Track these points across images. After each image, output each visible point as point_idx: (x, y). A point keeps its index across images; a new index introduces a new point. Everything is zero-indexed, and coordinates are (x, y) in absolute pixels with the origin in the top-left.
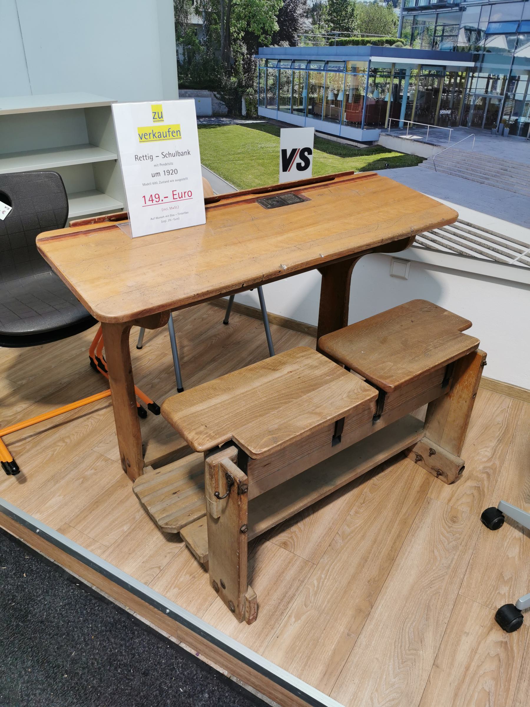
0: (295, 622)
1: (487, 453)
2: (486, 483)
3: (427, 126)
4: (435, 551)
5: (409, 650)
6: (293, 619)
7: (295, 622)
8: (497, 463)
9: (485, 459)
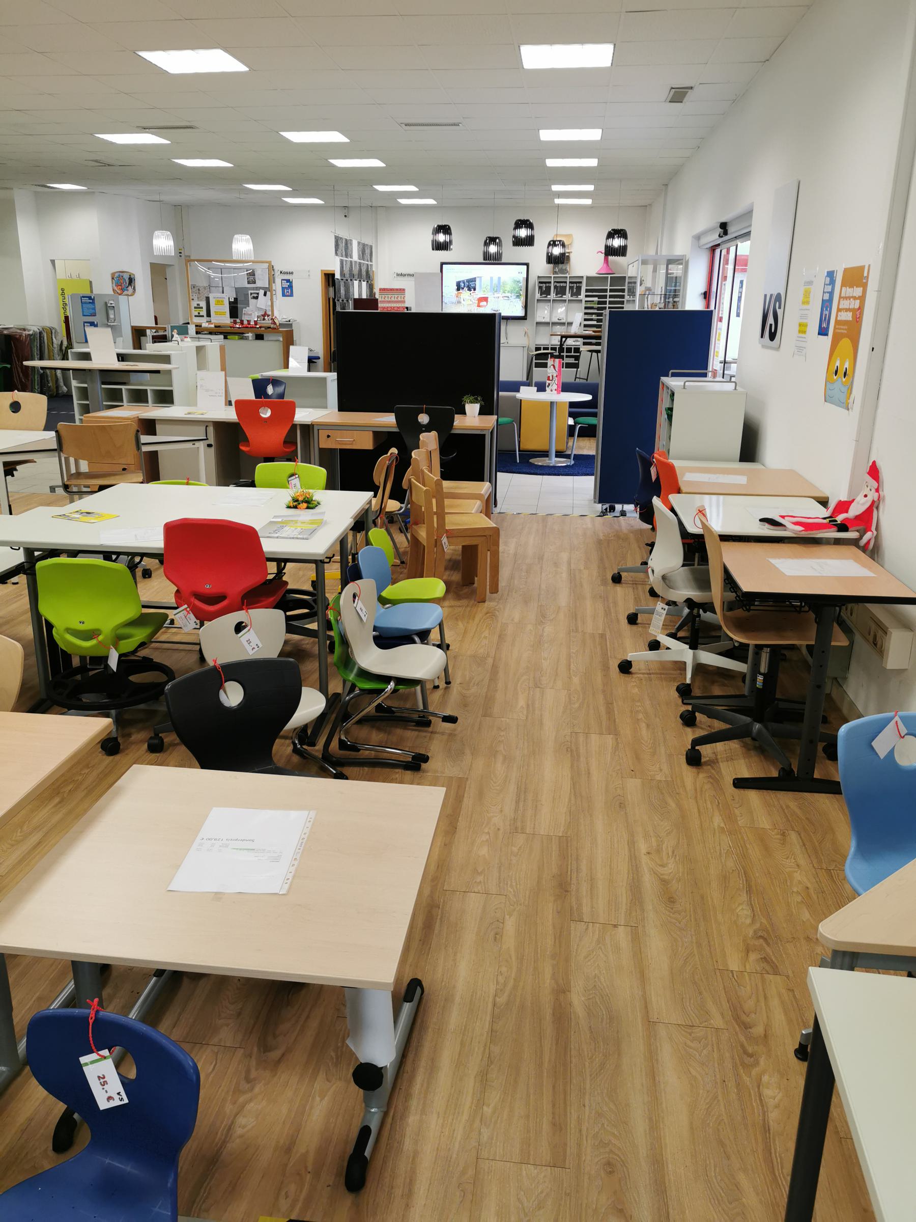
0: (321, 1100)
1: (745, 912)
2: (768, 949)
3: (574, 353)
4: (691, 1070)
5: (730, 1203)
6: (318, 1099)
7: (321, 1100)
8: (764, 921)
9: (749, 921)
